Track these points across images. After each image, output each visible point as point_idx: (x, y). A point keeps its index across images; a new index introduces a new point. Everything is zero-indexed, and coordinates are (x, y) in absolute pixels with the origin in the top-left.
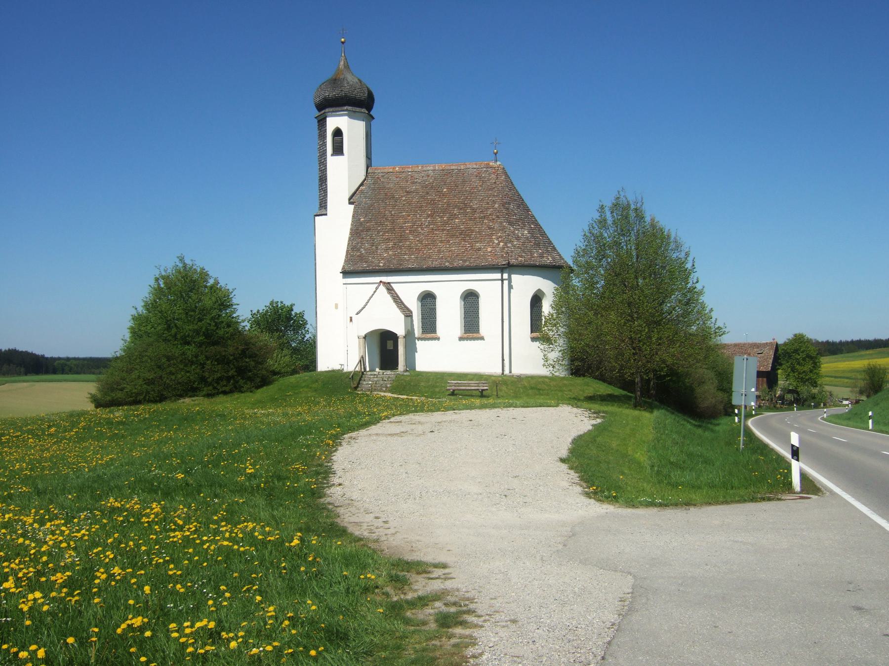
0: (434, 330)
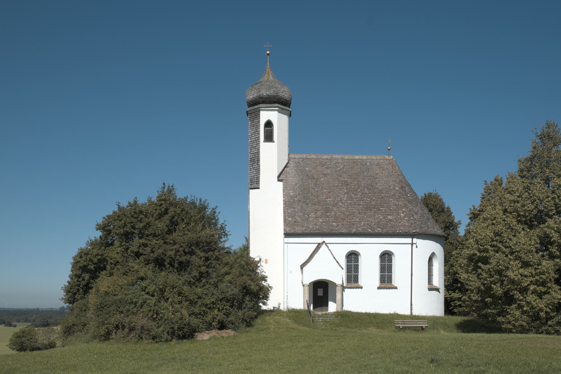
0: (356, 280)
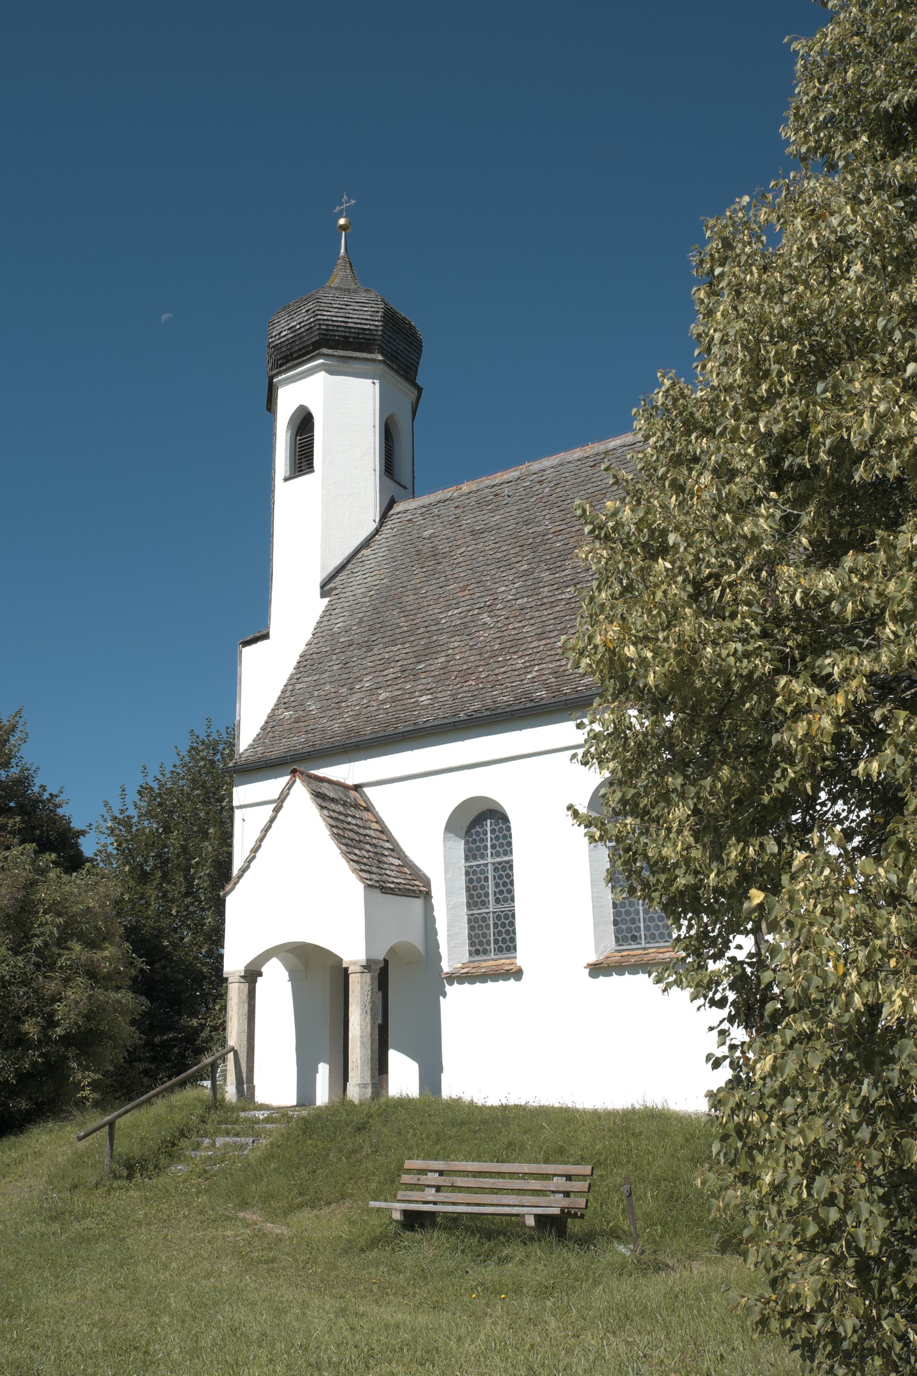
0: (507, 943)
